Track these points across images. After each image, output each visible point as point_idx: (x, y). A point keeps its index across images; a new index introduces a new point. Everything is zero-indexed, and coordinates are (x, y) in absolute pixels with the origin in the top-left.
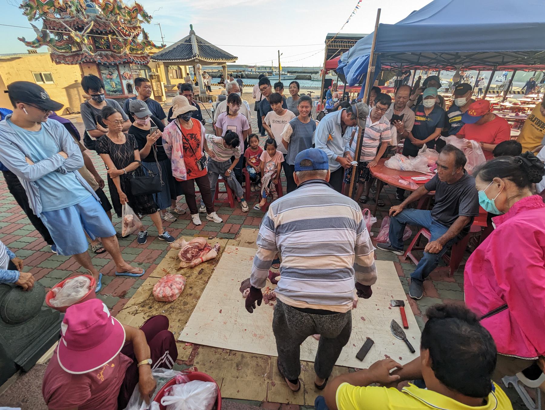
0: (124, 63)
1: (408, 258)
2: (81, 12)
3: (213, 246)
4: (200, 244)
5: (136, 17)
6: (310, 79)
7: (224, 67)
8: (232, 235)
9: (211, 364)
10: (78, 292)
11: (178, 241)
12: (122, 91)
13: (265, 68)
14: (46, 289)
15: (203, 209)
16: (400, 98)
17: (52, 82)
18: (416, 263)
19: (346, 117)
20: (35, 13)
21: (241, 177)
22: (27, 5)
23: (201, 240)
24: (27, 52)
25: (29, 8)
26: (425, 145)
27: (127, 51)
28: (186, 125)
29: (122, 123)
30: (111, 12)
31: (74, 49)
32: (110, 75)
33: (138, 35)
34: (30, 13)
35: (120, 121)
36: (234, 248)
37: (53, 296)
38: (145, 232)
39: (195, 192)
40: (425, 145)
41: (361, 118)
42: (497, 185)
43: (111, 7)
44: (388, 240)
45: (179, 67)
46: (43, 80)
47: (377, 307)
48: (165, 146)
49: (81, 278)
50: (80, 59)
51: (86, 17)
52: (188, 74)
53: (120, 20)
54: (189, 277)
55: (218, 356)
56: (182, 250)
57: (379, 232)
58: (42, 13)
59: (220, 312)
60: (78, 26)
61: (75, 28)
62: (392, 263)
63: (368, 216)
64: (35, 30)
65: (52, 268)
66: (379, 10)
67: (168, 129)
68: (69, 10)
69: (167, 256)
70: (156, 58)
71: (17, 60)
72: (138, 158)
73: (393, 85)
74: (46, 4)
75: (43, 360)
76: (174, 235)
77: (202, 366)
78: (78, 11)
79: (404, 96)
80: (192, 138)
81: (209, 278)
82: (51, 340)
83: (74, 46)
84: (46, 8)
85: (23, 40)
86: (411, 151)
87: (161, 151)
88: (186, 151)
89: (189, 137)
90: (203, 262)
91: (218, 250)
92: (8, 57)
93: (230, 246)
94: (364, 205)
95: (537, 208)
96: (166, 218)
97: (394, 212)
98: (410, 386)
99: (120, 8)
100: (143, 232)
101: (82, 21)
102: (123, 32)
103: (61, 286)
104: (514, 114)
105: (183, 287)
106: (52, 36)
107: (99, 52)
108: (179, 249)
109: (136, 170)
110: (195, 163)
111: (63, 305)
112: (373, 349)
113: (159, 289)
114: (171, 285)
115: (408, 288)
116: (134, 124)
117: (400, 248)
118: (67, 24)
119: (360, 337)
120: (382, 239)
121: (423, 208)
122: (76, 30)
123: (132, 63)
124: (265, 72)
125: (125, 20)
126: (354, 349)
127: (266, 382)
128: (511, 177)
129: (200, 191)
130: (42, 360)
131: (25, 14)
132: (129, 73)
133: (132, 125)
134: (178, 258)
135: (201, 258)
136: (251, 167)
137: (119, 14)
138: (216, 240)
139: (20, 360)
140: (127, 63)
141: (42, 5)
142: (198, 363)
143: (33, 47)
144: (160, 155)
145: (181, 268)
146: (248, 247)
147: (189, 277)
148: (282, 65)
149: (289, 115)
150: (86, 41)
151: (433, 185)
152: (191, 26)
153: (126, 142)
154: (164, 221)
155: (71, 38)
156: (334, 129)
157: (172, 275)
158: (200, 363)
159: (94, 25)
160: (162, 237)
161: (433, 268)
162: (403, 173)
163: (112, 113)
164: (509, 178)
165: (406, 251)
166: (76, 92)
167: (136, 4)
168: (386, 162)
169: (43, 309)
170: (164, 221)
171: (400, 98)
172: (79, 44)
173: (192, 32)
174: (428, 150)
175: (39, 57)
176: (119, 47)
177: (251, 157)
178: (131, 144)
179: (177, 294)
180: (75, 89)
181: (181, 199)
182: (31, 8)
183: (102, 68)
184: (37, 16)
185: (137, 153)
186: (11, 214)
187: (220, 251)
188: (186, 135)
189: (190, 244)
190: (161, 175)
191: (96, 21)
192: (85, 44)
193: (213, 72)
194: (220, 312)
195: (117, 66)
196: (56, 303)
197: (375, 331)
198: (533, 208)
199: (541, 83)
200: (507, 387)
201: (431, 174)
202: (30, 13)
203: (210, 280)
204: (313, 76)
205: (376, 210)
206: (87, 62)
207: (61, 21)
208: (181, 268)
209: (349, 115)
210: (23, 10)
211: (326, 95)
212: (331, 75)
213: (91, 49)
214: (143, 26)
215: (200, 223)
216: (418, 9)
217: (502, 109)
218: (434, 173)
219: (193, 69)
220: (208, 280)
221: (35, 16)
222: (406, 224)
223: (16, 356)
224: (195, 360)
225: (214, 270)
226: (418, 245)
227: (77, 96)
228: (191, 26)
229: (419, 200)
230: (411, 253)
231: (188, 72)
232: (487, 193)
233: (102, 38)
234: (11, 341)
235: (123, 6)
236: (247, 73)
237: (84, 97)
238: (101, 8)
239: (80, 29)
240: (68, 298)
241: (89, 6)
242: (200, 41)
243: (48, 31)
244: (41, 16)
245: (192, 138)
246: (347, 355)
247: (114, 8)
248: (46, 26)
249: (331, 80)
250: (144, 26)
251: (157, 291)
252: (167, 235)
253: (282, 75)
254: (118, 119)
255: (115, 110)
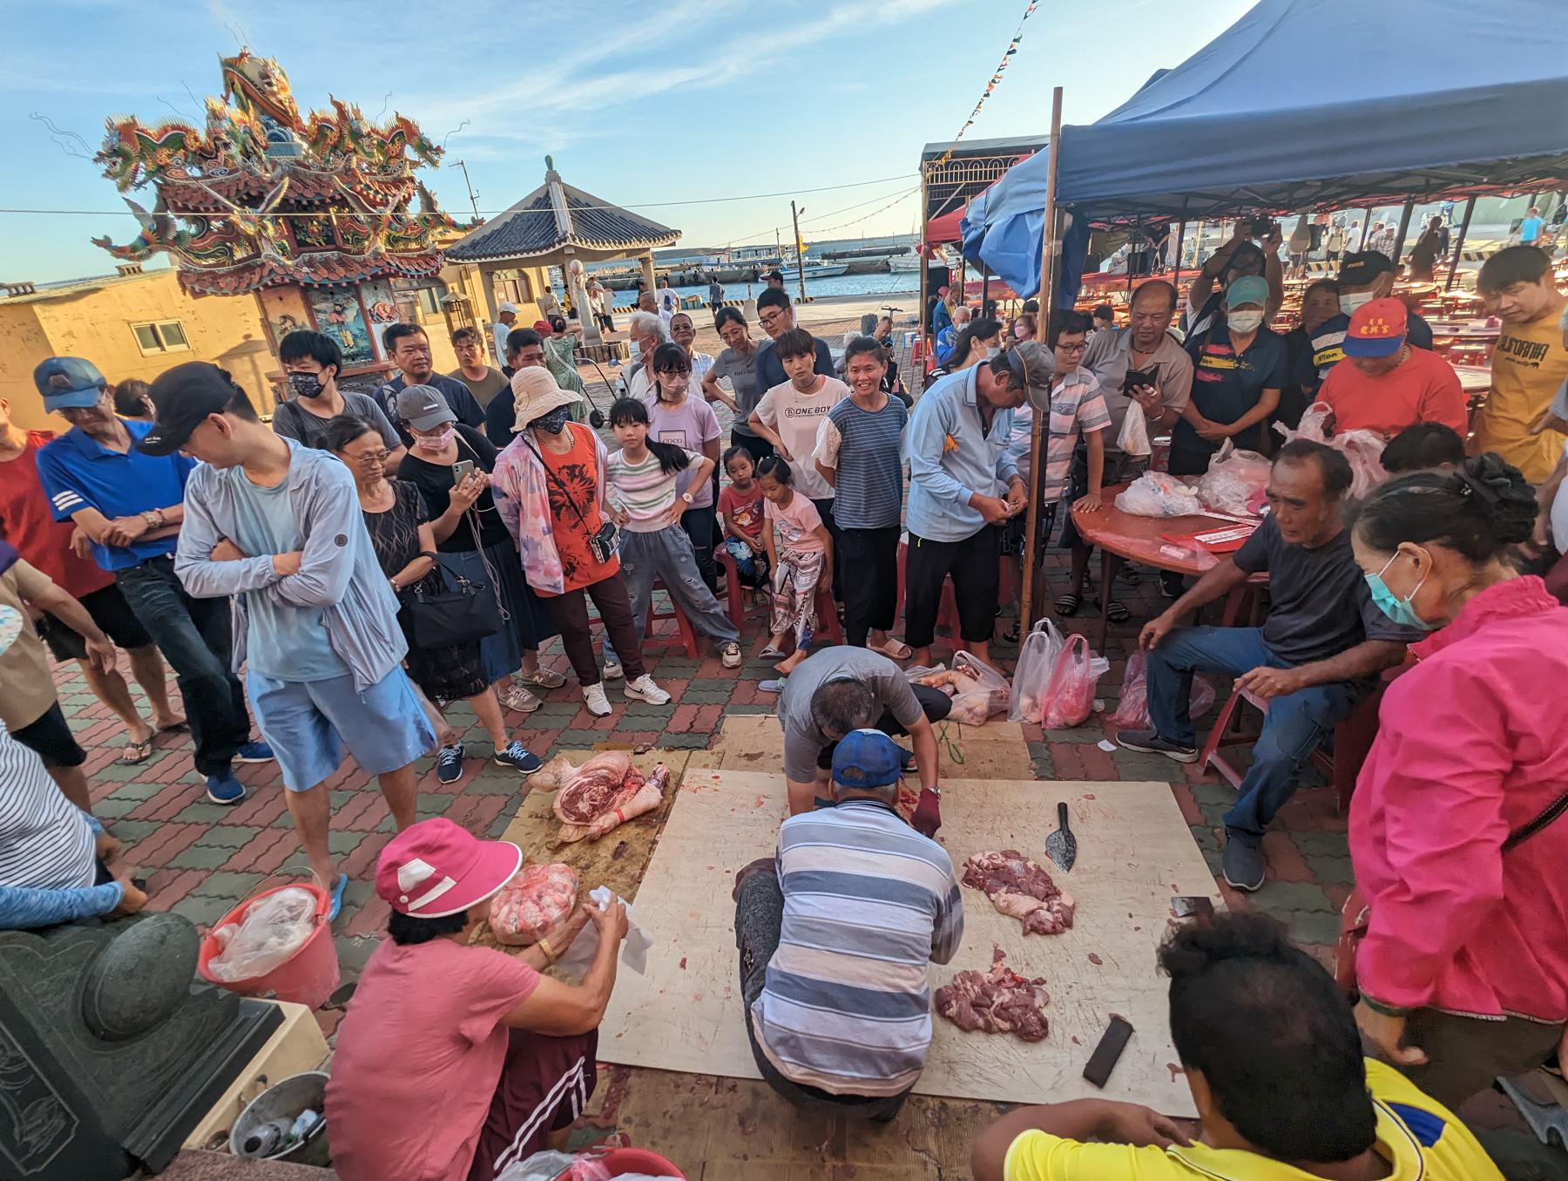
0: (375, 277)
1: (1211, 770)
2: (254, 158)
3: (647, 772)
4: (613, 771)
5: (400, 155)
6: (886, 269)
7: (644, 261)
8: (700, 738)
9: (668, 1123)
10: (283, 935)
11: (551, 766)
12: (372, 353)
13: (756, 252)
14: (200, 930)
15: (612, 668)
16: (1143, 316)
17: (183, 347)
18: (1237, 783)
19: (994, 385)
20: (136, 170)
21: (711, 570)
22: (115, 152)
23: (612, 761)
24: (117, 272)
25: (120, 160)
26: (1227, 440)
27: (382, 246)
28: (555, 442)
29: (382, 458)
30: (335, 147)
31: (239, 254)
32: (339, 313)
33: (407, 200)
34: (123, 170)
35: (378, 453)
36: (708, 774)
37: (218, 949)
38: (456, 747)
39: (588, 622)
40: (1227, 440)
41: (1035, 385)
42: (1410, 560)
43: (333, 136)
44: (1148, 720)
45: (520, 272)
46: (159, 344)
47: (1134, 923)
48: (500, 505)
49: (292, 895)
50: (256, 278)
51: (269, 167)
52: (548, 290)
53: (358, 165)
54: (587, 867)
55: (685, 1095)
56: (562, 791)
57: (1118, 700)
58: (152, 168)
59: (683, 965)
60: (248, 194)
61: (241, 199)
62: (1165, 787)
63: (1084, 655)
64: (137, 217)
65: (207, 869)
66: (1058, 92)
67: (506, 459)
68: (223, 153)
69: (522, 813)
70: (458, 254)
71: (91, 297)
72: (429, 544)
73: (1123, 268)
74: (164, 144)
75: (199, 1138)
76: (538, 749)
77: (640, 1129)
78: (247, 154)
79: (1153, 311)
80: (573, 476)
81: (644, 868)
82: (220, 1077)
83: (239, 245)
84: (163, 156)
85: (105, 243)
86: (1187, 459)
87: (492, 520)
88: (558, 514)
89: (564, 476)
90: (624, 823)
91: (664, 784)
92: (67, 291)
93: (697, 771)
94: (1068, 620)
95: (1522, 615)
96: (512, 702)
97: (1152, 635)
98: (1192, 1146)
99: (357, 135)
100: (450, 747)
101: (259, 179)
102: (366, 198)
103: (239, 919)
104: (1482, 323)
105: (573, 898)
106: (181, 225)
107: (306, 256)
108: (554, 788)
109: (426, 578)
110: (584, 545)
111: (246, 976)
112: (1131, 1048)
113: (506, 909)
114: (540, 897)
115: (1218, 857)
116: (412, 452)
117: (1186, 740)
118: (219, 192)
119: (1090, 1014)
120: (1130, 717)
121: (1240, 622)
122: (243, 204)
123: (395, 275)
124: (755, 263)
125: (370, 165)
126: (1075, 1053)
127: (829, 1165)
128: (1447, 538)
129: (603, 619)
130: (197, 1137)
131: (108, 174)
132: (389, 303)
133: (408, 455)
134: (553, 816)
135: (618, 811)
136: (739, 540)
137: (355, 151)
138: (655, 755)
139: (137, 1142)
140: (381, 279)
141: (154, 148)
142: (628, 1121)
143: (130, 258)
144: (490, 529)
145: (564, 844)
146: (746, 768)
147: (587, 867)
148: (805, 239)
149: (834, 391)
150: (271, 231)
151: (1259, 552)
152: (549, 160)
153: (396, 506)
154: (507, 710)
155: (230, 226)
156: (960, 421)
157: (539, 867)
158: (636, 1120)
159: (290, 187)
160: (504, 758)
161: (1286, 794)
162: (1172, 526)
163: (357, 433)
164: (1440, 540)
165: (1202, 749)
166: (249, 367)
167: (399, 119)
168: (1119, 496)
169: (196, 990)
170: (507, 710)
171: (1143, 316)
172: (252, 241)
173: (553, 177)
174: (1235, 453)
175: (149, 283)
176: (359, 239)
177: (738, 510)
178: (408, 509)
179: (558, 920)
180: (246, 358)
181: (551, 650)
182: (127, 158)
183: (314, 296)
184: (140, 177)
185: (426, 532)
186: (89, 723)
187: (669, 786)
188: (555, 471)
189: (584, 773)
190: (498, 594)
191: (294, 175)
192: (268, 239)
193: (614, 276)
194: (683, 965)
195: (356, 287)
196: (228, 970)
197: (1133, 994)
198: (1514, 614)
199: (1555, 221)
200: (1545, 1141)
201: (1252, 522)
202: (123, 170)
203: (647, 874)
204: (895, 260)
205: (1106, 634)
206: (276, 286)
207: (204, 185)
208: (564, 844)
209: (1000, 378)
210: (103, 167)
211: (933, 320)
212: (947, 257)
213: (283, 248)
214: (419, 174)
215: (607, 708)
216: (1172, 65)
217: (1449, 309)
218: (1259, 517)
219: (559, 271)
220: (641, 875)
221: (134, 178)
222: (1192, 671)
223: (128, 1131)
224: (622, 1113)
225: (655, 842)
226: (1236, 729)
227: (253, 377)
228: (549, 160)
229: (1227, 596)
230: (1219, 754)
231: (547, 283)
232: (1389, 581)
233: (311, 219)
234: (112, 1089)
235: (365, 130)
236: (707, 269)
237: (271, 380)
238: (308, 141)
239: (253, 201)
240: (260, 954)
241: (274, 137)
242: (576, 200)
243: (170, 214)
244: (150, 175)
245: (573, 476)
246: (1056, 1071)
247: (341, 137)
248: (163, 204)
249: (945, 271)
250: (422, 174)
251: (502, 916)
252: (517, 751)
253: (809, 265)
254: (371, 449)
255: (365, 425)
